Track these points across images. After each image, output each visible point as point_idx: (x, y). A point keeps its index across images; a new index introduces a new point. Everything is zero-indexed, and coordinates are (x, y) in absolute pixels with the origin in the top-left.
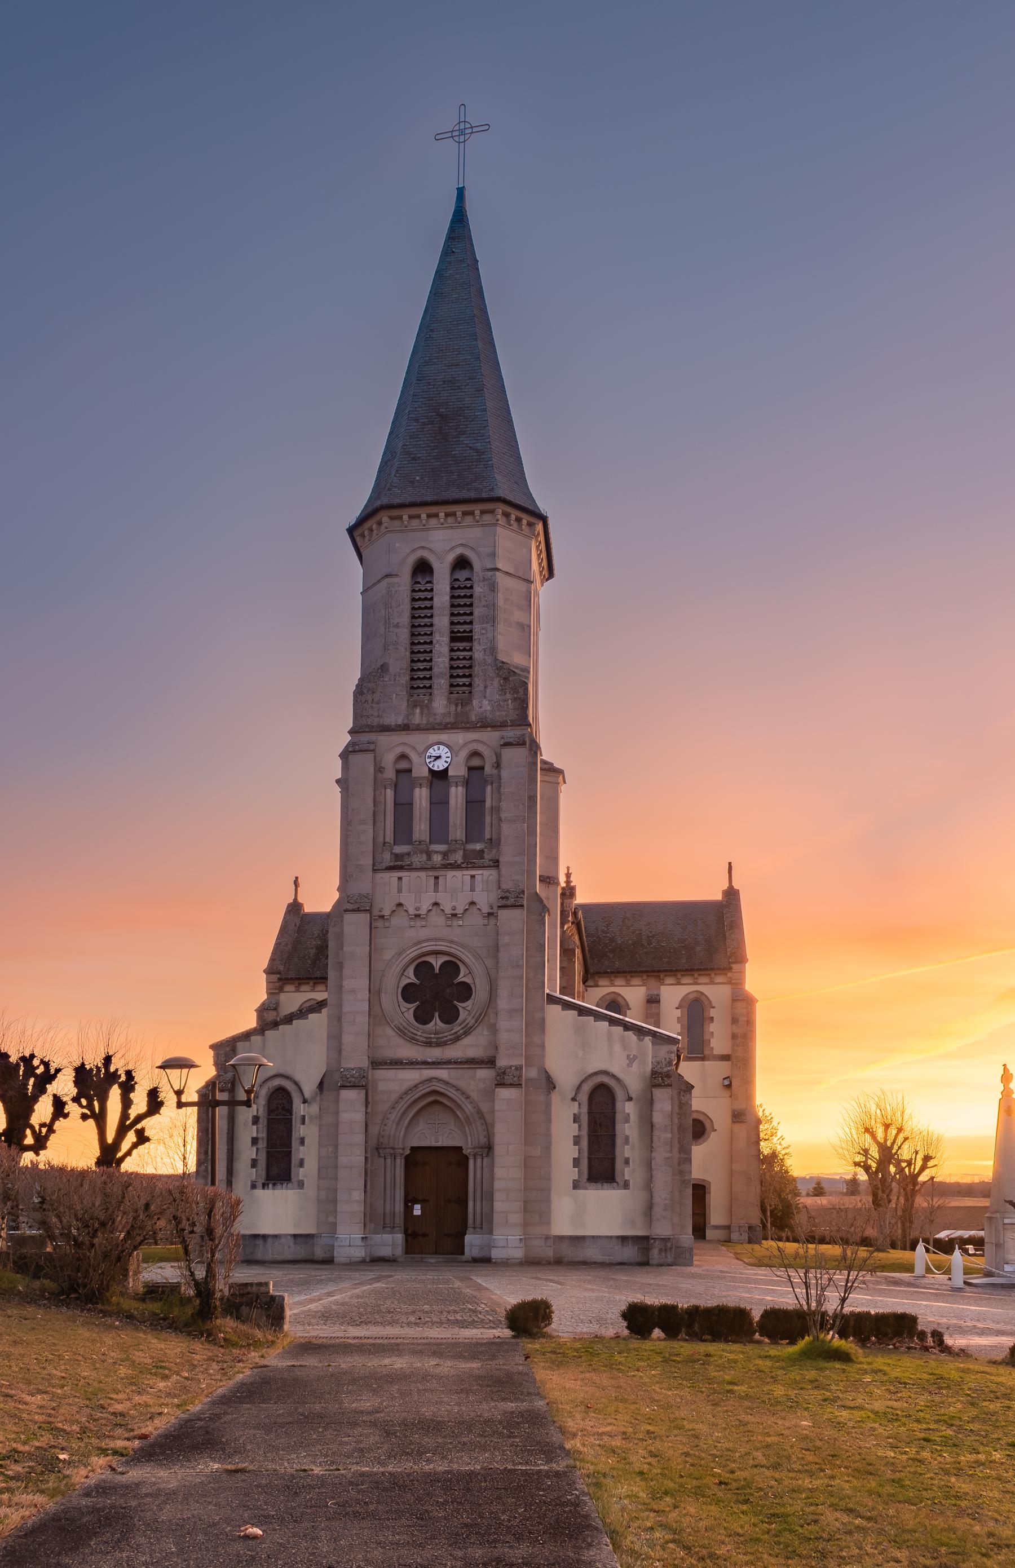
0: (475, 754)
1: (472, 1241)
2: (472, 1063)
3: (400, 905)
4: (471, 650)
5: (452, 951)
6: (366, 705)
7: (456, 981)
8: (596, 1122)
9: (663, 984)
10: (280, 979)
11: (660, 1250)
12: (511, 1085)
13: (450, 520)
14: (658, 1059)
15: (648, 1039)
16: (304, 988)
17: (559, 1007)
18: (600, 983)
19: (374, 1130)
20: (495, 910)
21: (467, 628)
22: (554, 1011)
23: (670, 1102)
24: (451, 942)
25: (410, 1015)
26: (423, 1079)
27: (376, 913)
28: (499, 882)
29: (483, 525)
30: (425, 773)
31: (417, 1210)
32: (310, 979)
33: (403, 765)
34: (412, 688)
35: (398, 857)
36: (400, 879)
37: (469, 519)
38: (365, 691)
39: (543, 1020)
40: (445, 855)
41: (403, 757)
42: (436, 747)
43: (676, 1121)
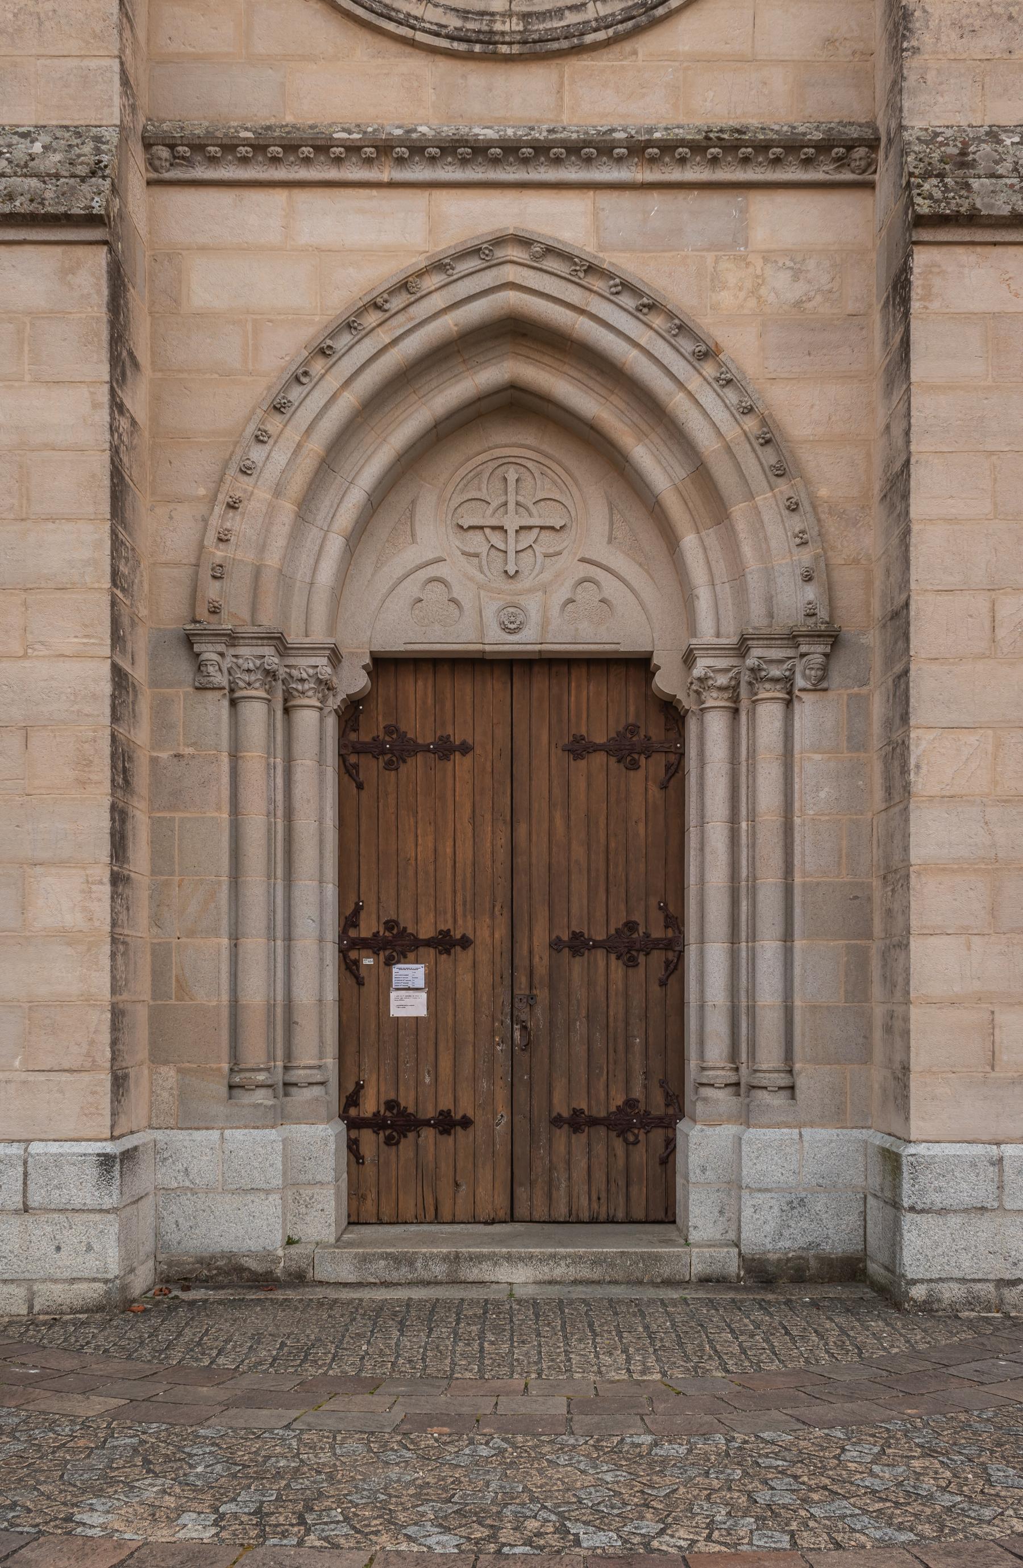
1: (752, 1175)
19: (169, 535)
26: (449, 240)
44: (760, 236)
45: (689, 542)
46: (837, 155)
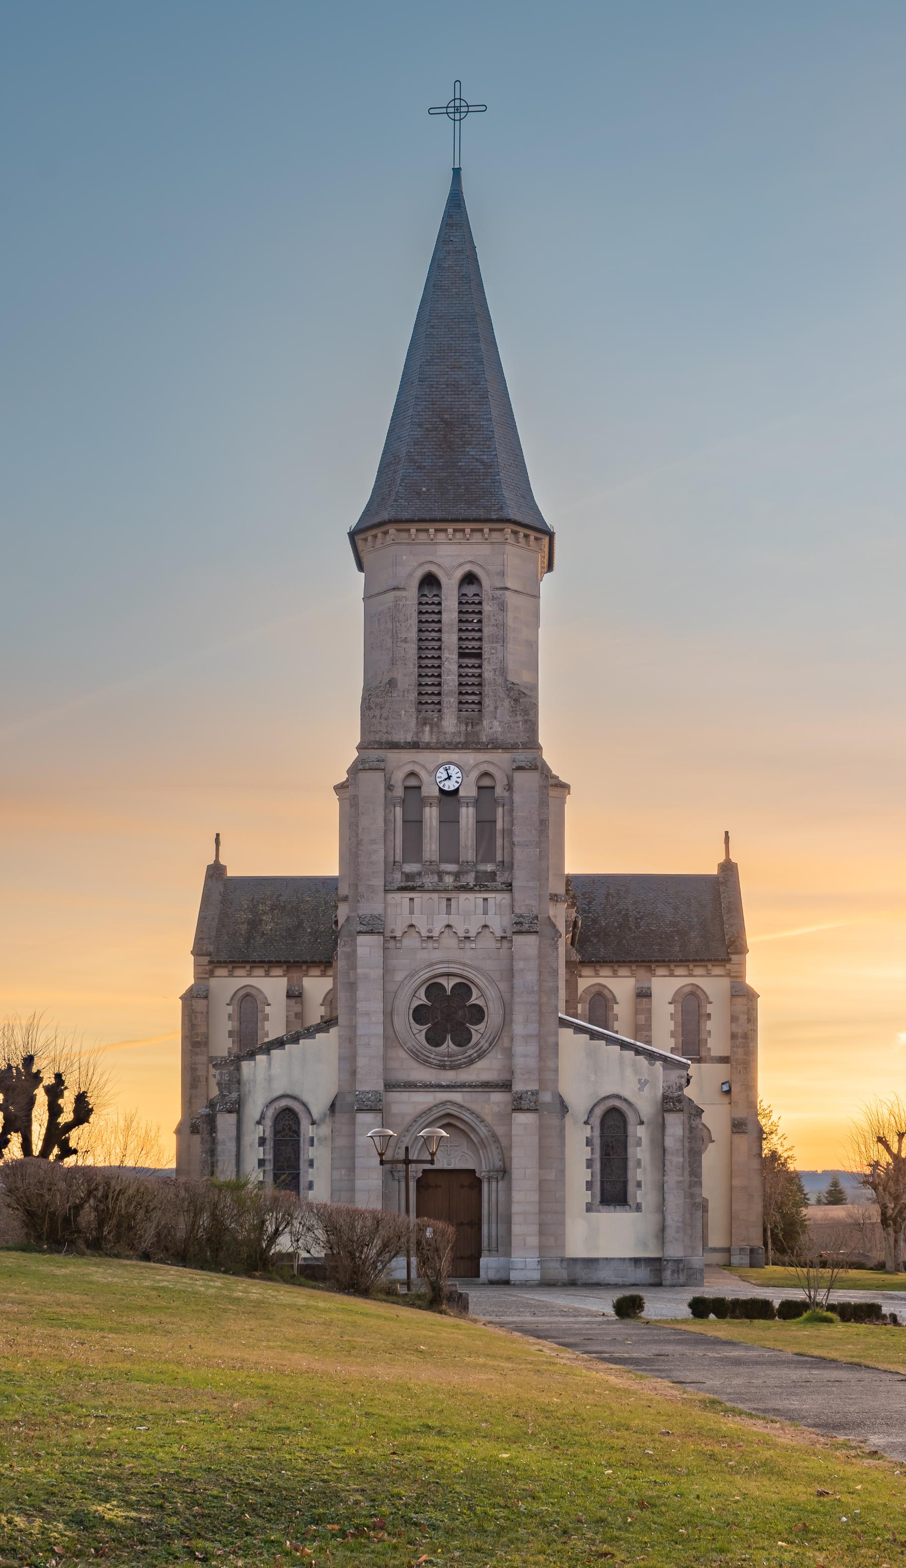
0: (486, 774)
1: (488, 1264)
2: (486, 1086)
4: (480, 667)
5: (465, 973)
6: (374, 720)
7: (468, 1004)
9: (654, 975)
10: (211, 962)
11: (673, 1272)
14: (669, 1083)
15: (659, 1064)
17: (571, 1031)
18: (583, 974)
20: (509, 934)
21: (476, 644)
22: (566, 1034)
23: (681, 1127)
24: (464, 964)
25: (422, 1037)
26: (437, 1102)
27: (388, 934)
28: (512, 906)
30: (436, 793)
32: (247, 962)
33: (412, 782)
34: (420, 703)
35: (409, 877)
36: (412, 899)
38: (373, 706)
39: (557, 1044)
40: (457, 875)
41: (412, 774)
43: (687, 1145)
45: (481, 1151)
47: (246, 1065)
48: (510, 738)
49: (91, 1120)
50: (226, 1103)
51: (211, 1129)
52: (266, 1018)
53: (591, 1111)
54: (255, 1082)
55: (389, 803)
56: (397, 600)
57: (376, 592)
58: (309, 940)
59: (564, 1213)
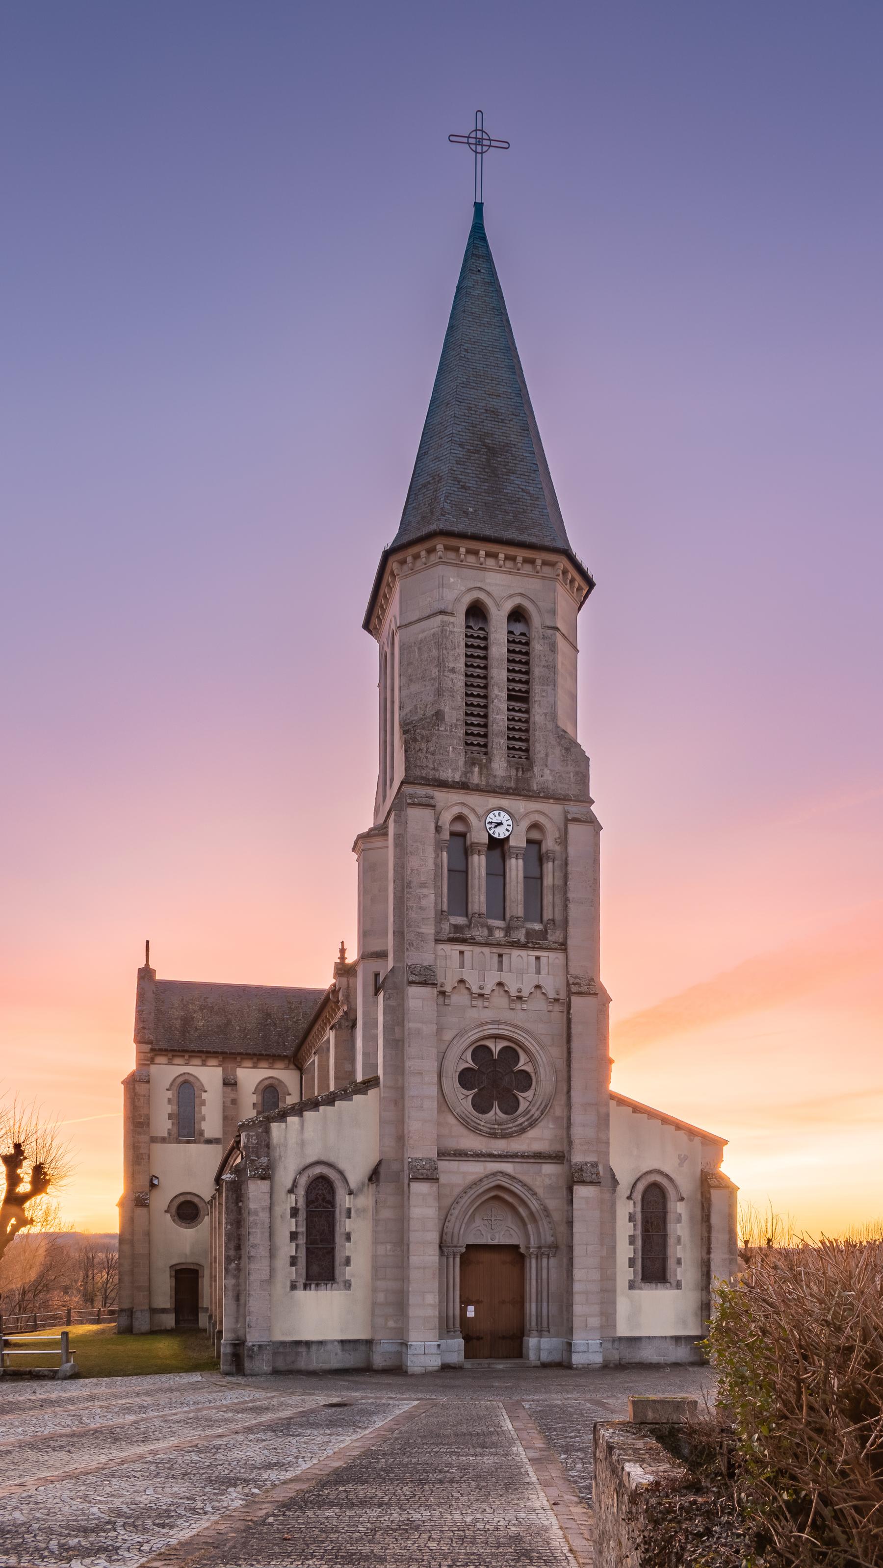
0: (535, 826)
1: (540, 1347)
2: (539, 1157)
3: (462, 981)
8: (647, 1222)
10: (152, 1050)
12: (591, 1183)
13: (509, 564)
16: (177, 1061)
21: (523, 687)
24: (515, 1026)
26: (488, 1172)
29: (543, 578)
30: (486, 840)
31: (471, 1312)
35: (457, 928)
37: (528, 568)
38: (419, 738)
41: (460, 818)
42: (496, 812)
44: (543, 1171)
45: (529, 1226)
46: (559, 1157)
47: (275, 1127)
48: (561, 788)
49: (48, 1190)
50: (257, 1169)
51: (237, 1198)
52: (203, 1103)
53: (634, 1187)
54: (286, 1147)
55: (439, 846)
56: (444, 625)
57: (415, 618)
58: (240, 1036)
59: (615, 1291)
